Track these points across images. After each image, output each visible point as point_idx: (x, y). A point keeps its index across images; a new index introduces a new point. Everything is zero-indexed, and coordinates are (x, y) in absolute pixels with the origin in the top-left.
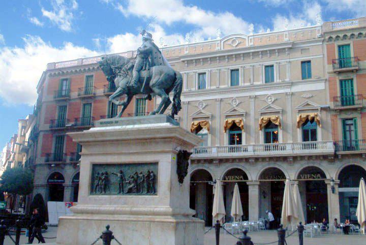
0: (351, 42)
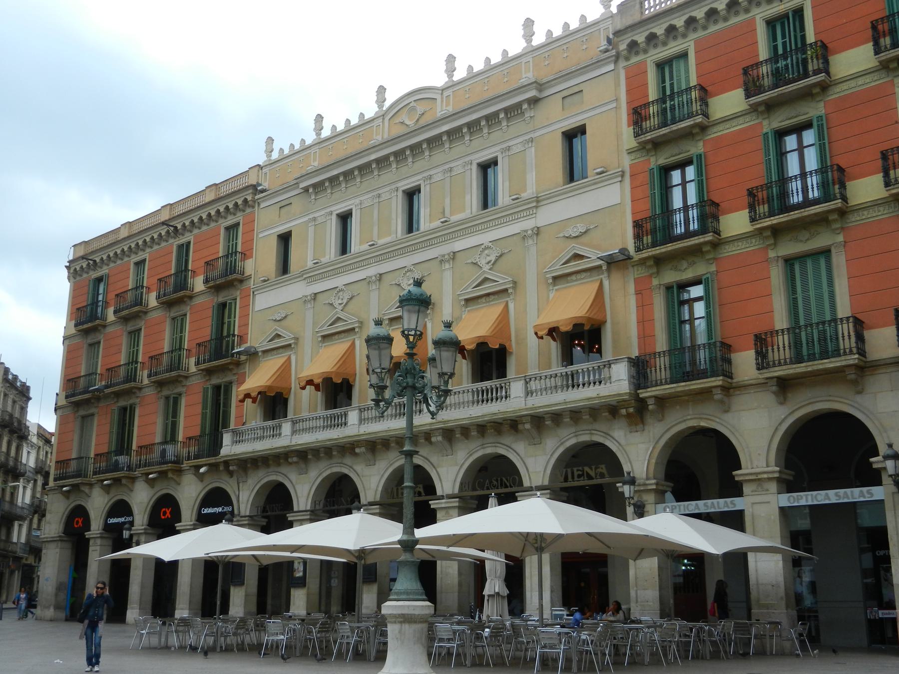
0: (689, 44)
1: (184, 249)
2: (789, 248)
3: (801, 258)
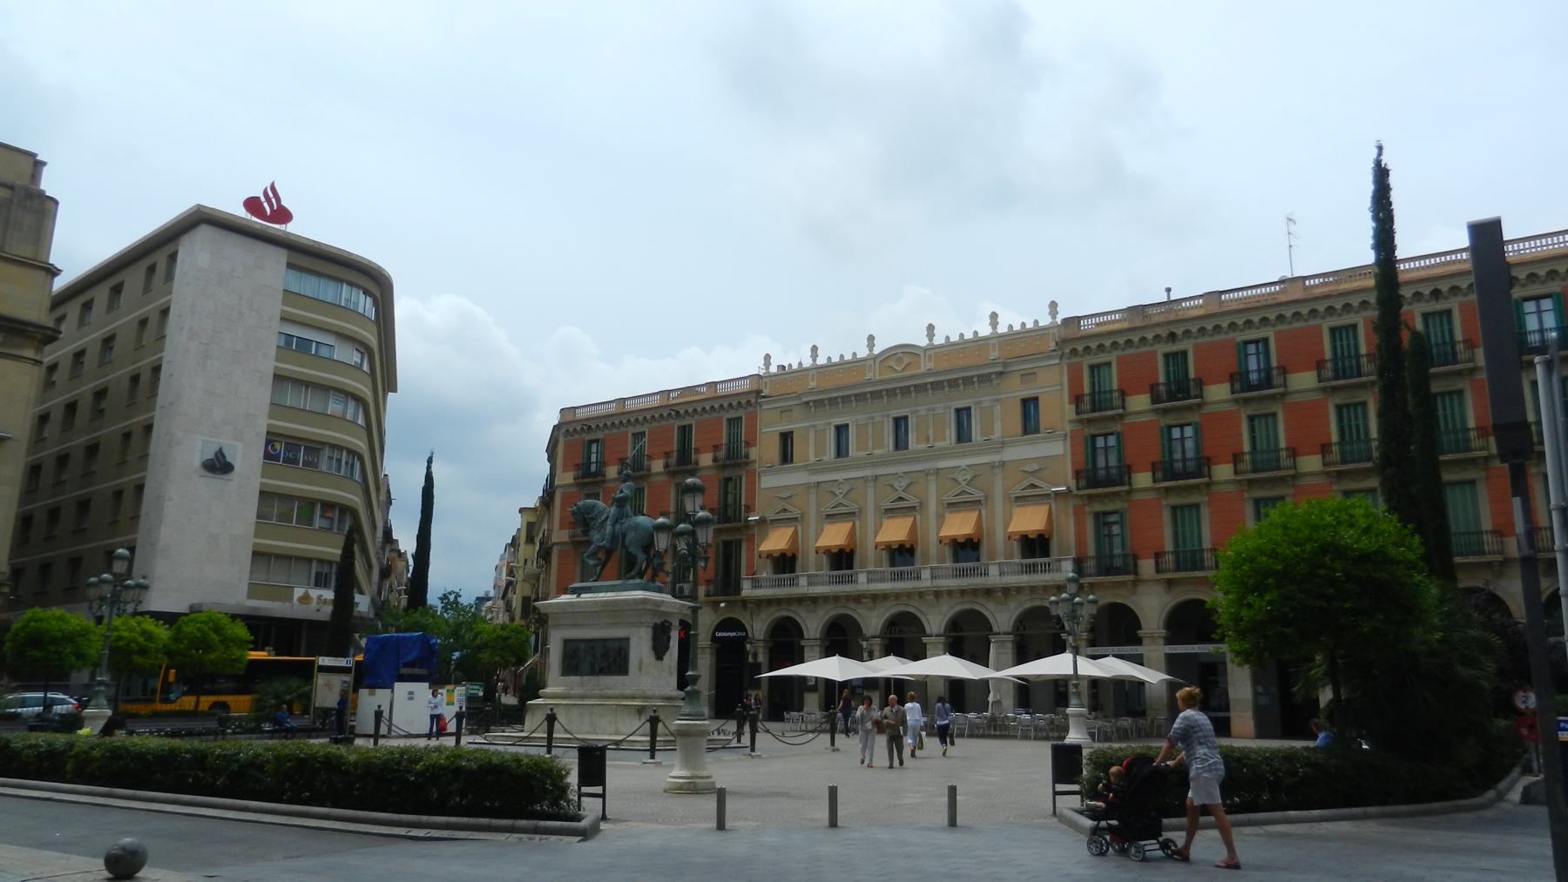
0: (1112, 357)
1: (685, 431)
2: (1175, 500)
3: (1182, 507)
